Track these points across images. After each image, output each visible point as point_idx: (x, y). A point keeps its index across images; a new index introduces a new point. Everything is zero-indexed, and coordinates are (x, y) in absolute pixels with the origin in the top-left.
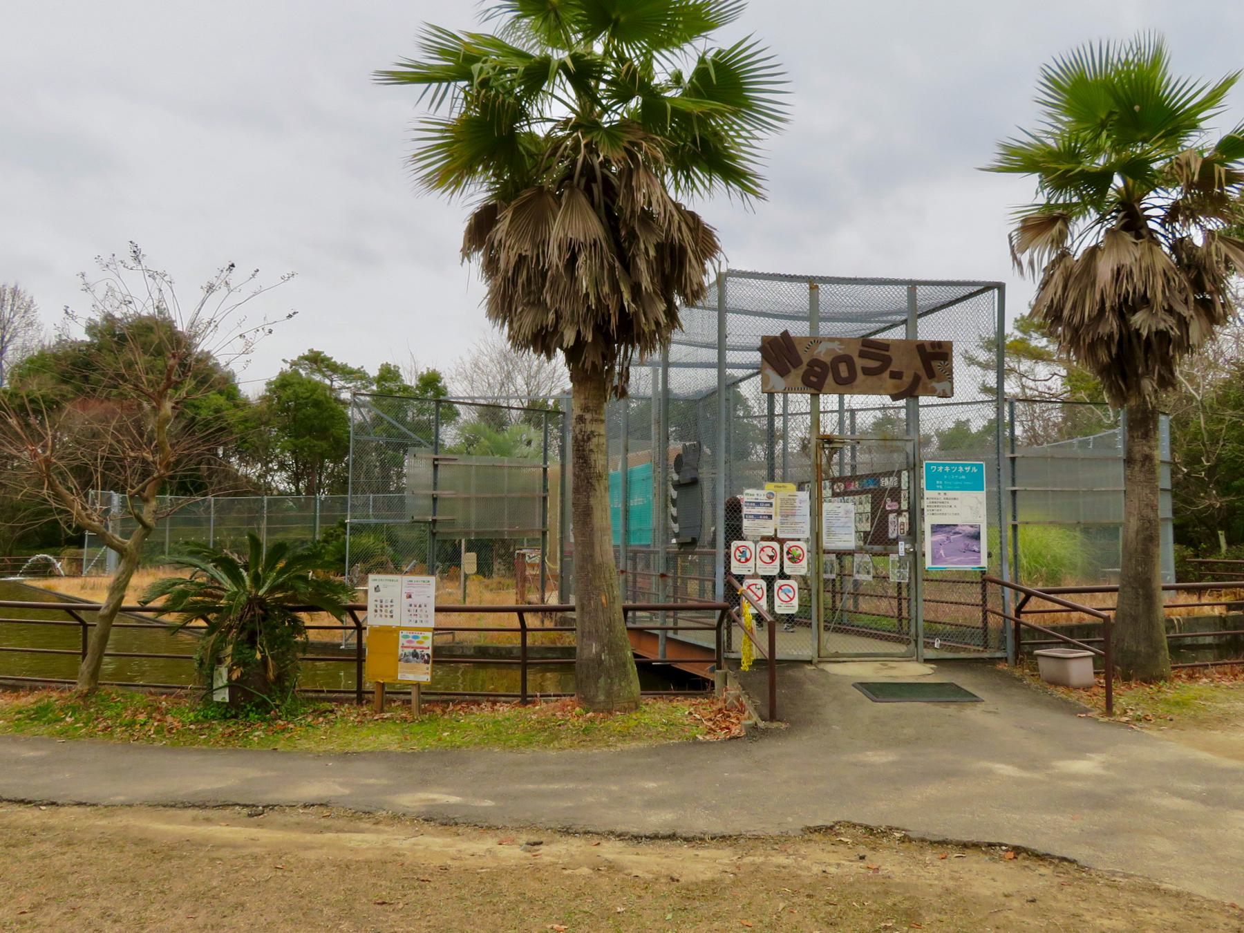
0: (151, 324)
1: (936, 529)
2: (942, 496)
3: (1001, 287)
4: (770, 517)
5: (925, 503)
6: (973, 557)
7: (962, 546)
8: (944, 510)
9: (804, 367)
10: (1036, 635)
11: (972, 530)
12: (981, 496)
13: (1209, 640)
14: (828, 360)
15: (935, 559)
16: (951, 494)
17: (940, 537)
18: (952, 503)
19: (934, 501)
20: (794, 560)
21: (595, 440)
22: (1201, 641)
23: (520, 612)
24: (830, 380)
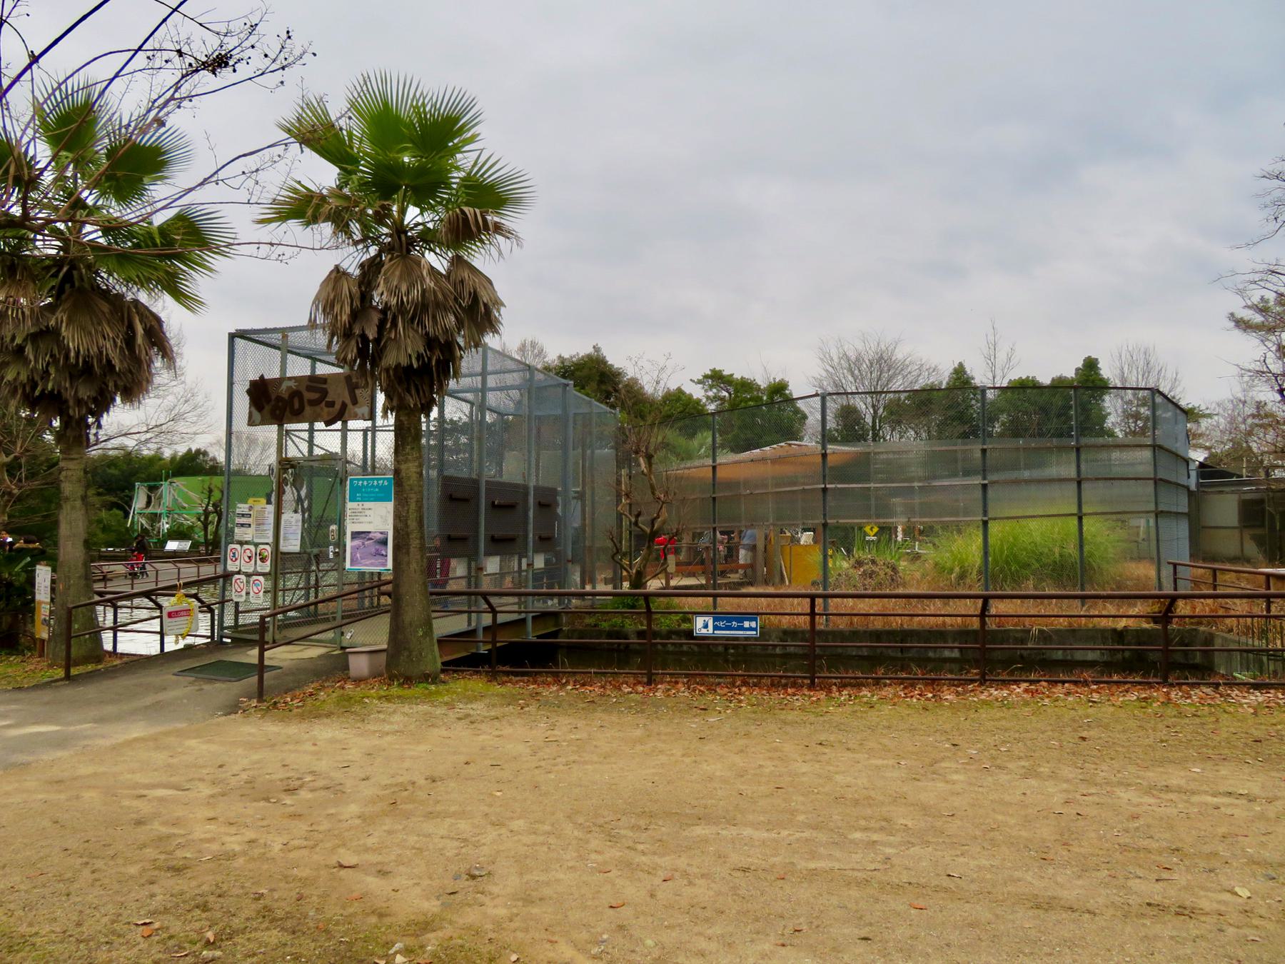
0: (581, 364)
1: (356, 535)
2: (361, 507)
3: (232, 337)
4: (250, 525)
5: (348, 512)
6: (381, 560)
7: (373, 550)
8: (362, 519)
9: (273, 403)
10: (830, 637)
11: (379, 536)
12: (390, 506)
13: (1091, 656)
14: (286, 396)
15: (353, 562)
16: (367, 505)
17: (357, 542)
18: (368, 512)
19: (354, 511)
20: (263, 560)
21: (64, 473)
22: (1079, 656)
23: (813, 598)
24: (287, 413)
